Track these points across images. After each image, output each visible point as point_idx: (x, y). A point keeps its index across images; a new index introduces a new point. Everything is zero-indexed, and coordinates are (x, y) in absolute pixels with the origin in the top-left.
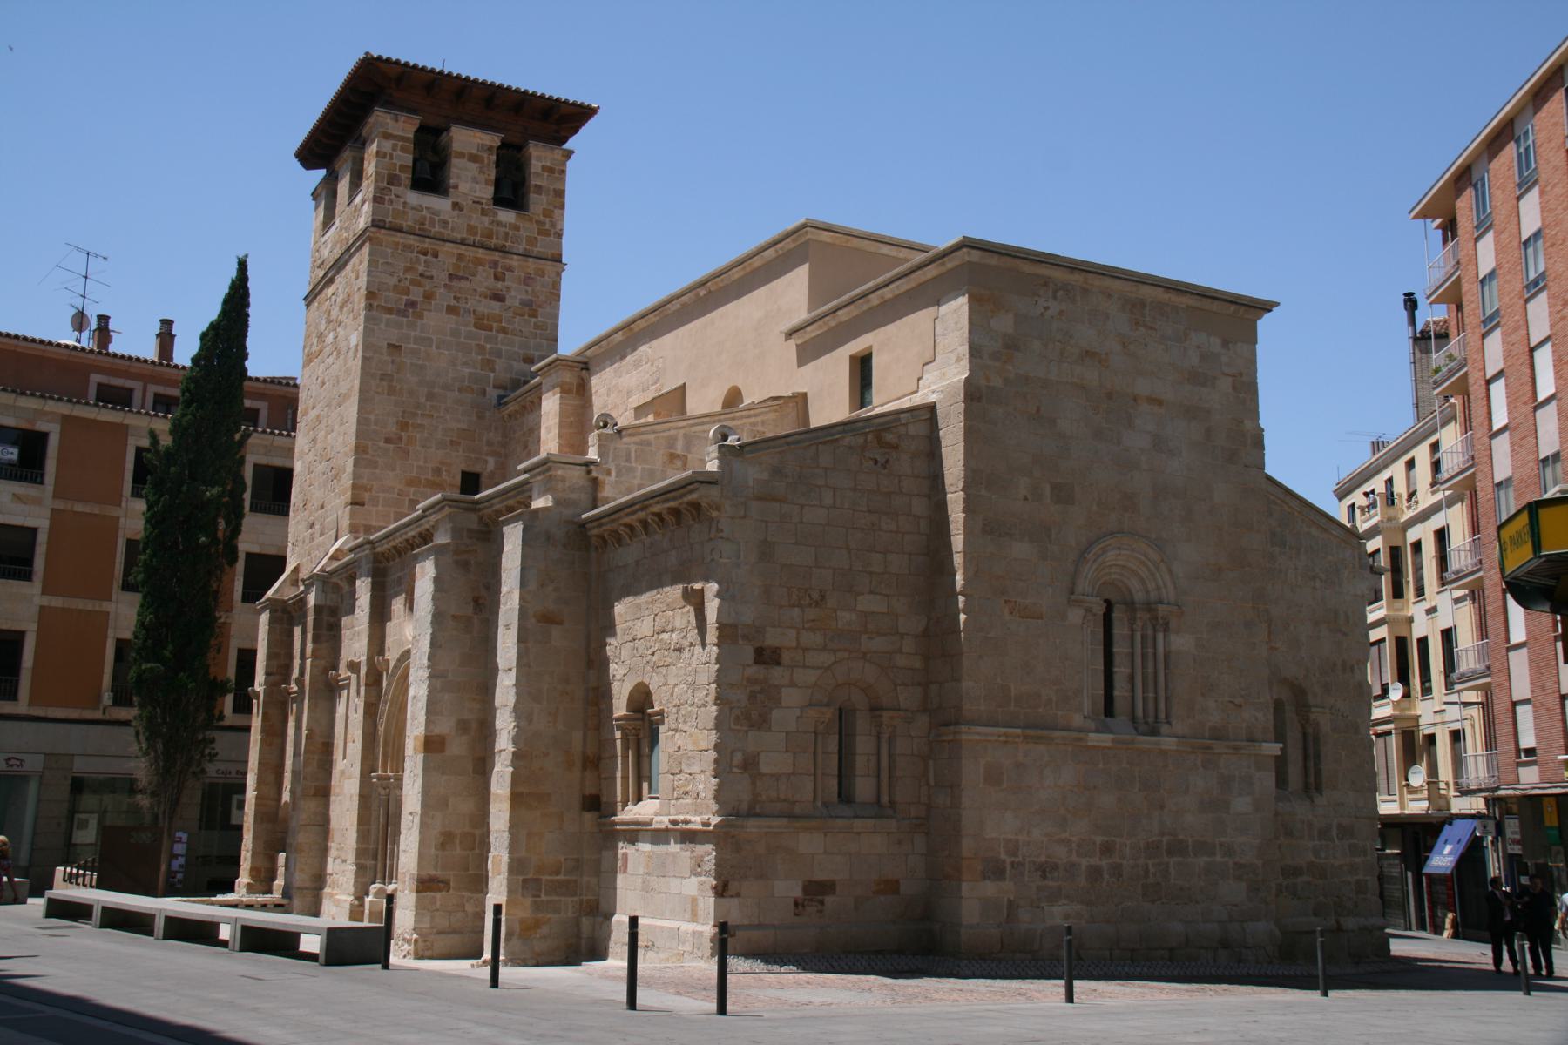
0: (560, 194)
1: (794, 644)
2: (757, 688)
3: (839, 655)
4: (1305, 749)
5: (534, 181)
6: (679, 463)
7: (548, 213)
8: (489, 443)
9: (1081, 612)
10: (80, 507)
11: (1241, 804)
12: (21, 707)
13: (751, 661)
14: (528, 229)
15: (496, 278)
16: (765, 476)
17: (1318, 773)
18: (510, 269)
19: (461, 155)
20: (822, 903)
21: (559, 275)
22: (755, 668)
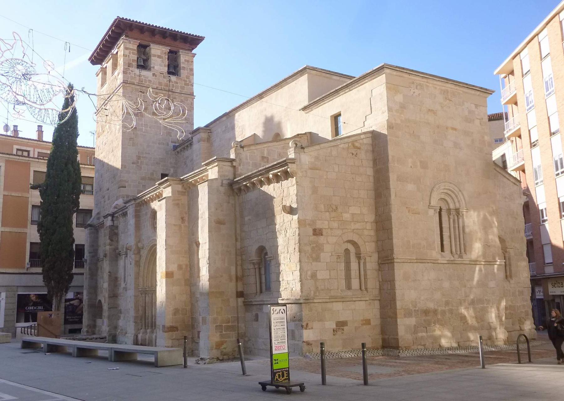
0: (192, 70)
2: (314, 245)
5: (182, 65)
6: (265, 160)
7: (188, 77)
8: (171, 163)
10: (13, 194)
14: (181, 84)
16: (313, 160)
17: (510, 271)
19: (155, 56)
20: (343, 330)
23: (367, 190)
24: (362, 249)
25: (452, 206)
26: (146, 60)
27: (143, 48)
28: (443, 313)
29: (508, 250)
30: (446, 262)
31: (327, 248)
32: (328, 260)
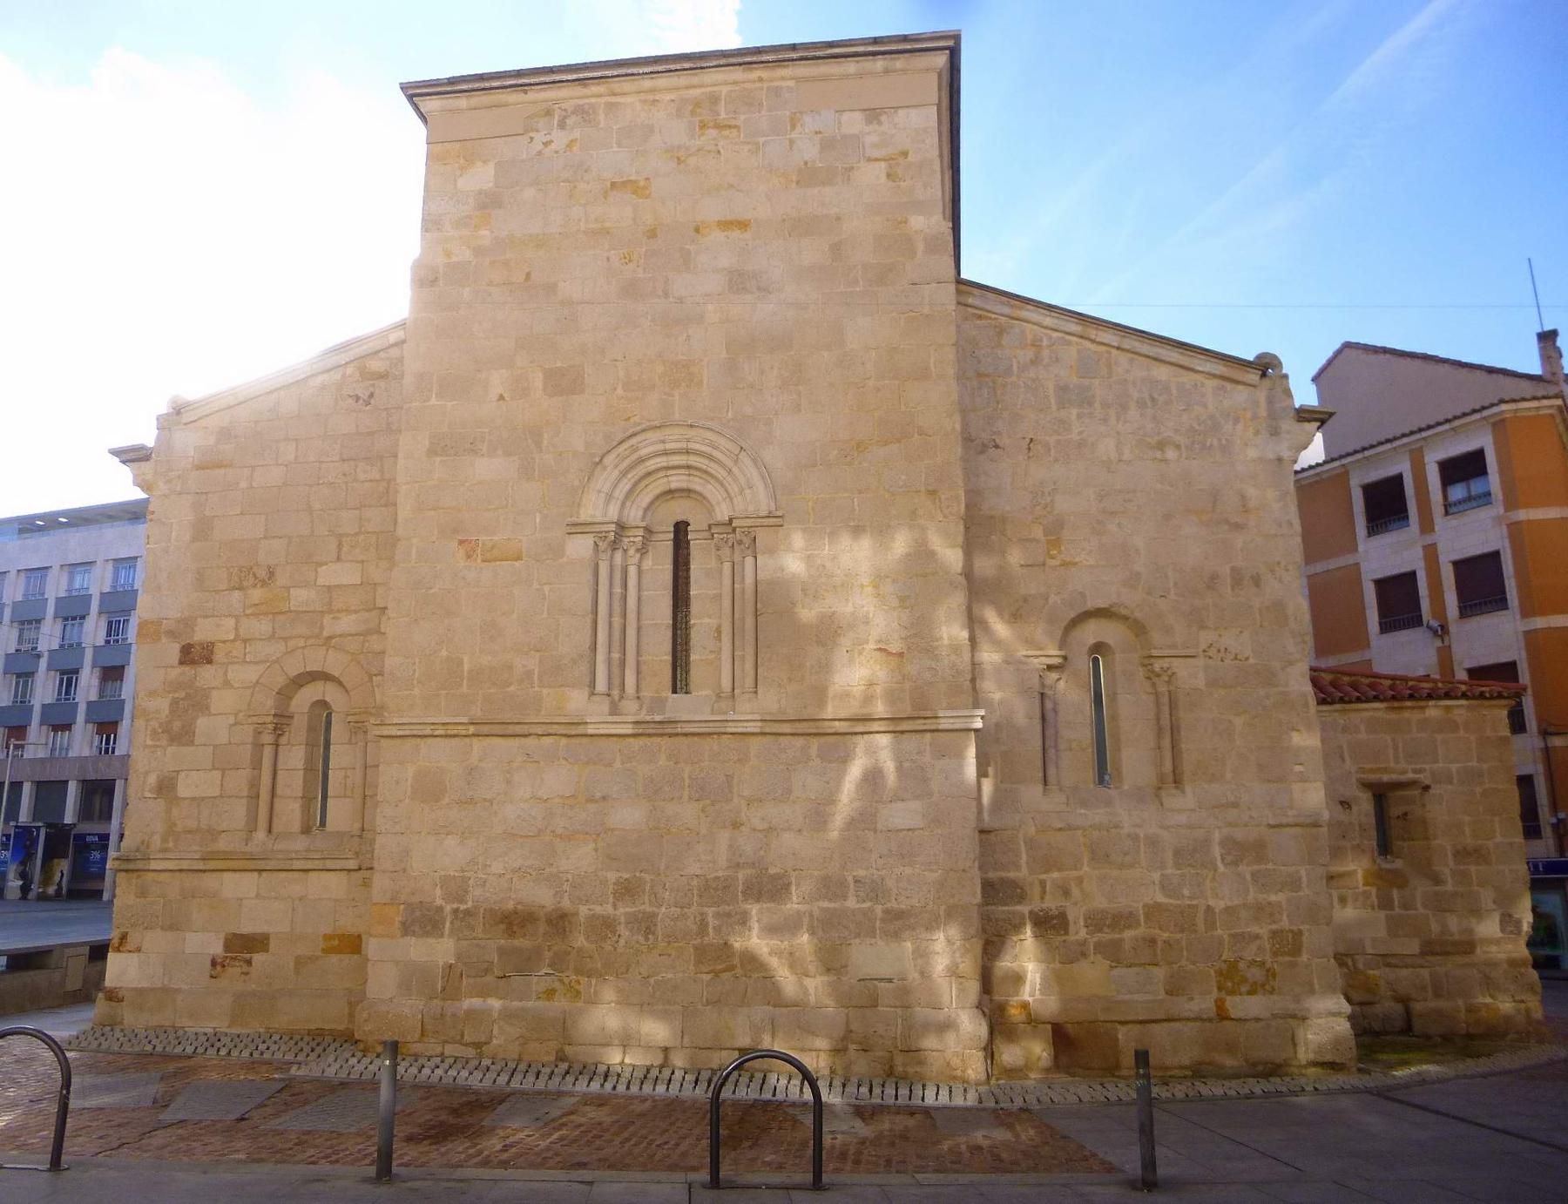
20: (249, 962)
28: (604, 927)
30: (628, 729)
31: (222, 701)
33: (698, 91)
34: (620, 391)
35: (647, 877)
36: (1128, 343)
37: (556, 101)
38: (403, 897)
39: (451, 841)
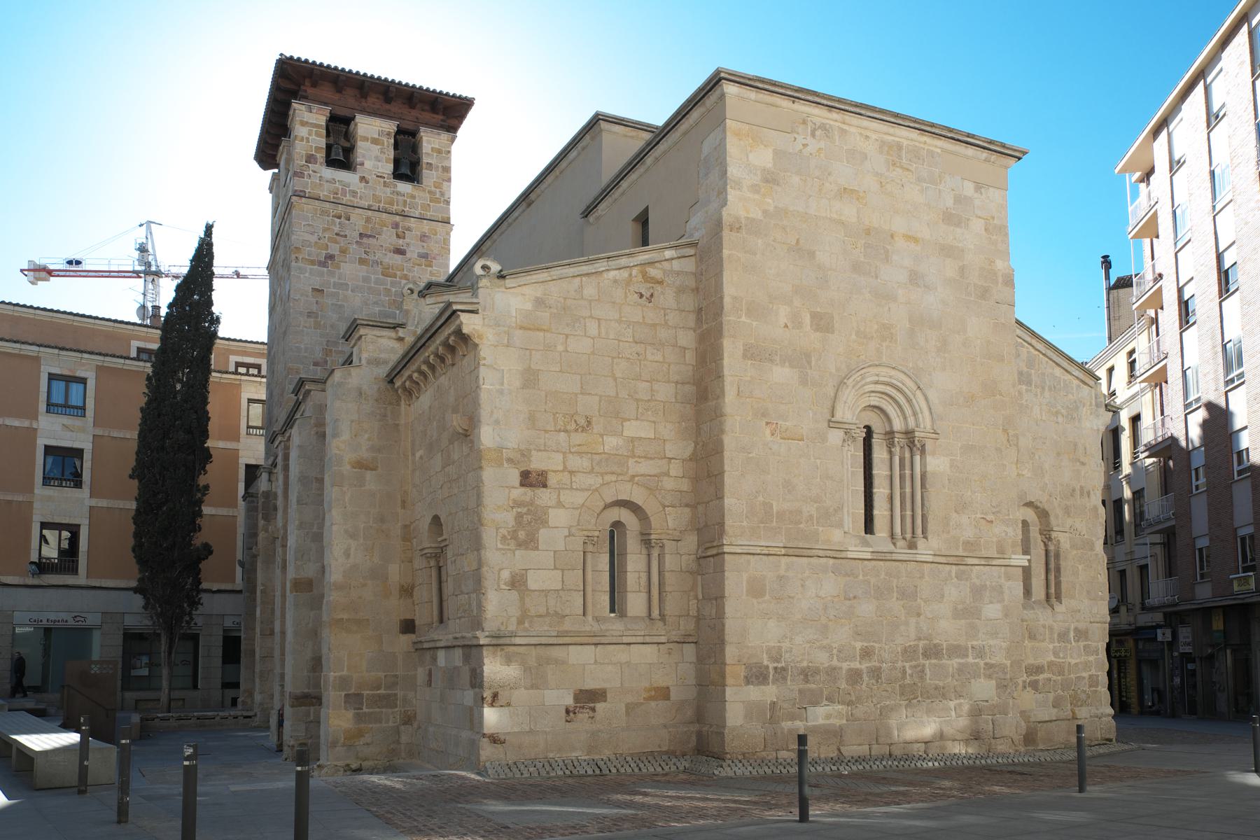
0: (447, 170)
1: (561, 468)
3: (608, 478)
4: (1047, 564)
5: (425, 160)
9: (841, 433)
10: (115, 434)
11: (992, 610)
12: (81, 579)
13: (517, 483)
15: (398, 236)
16: (529, 306)
17: (1058, 584)
18: (409, 229)
19: (366, 139)
20: (593, 710)
21: (448, 234)
22: (523, 490)
23: (677, 383)
24: (655, 522)
25: (898, 425)
26: (349, 151)
27: (339, 127)
28: (855, 676)
29: (1054, 535)
30: (869, 556)
31: (559, 518)
32: (560, 546)
33: (891, 138)
34: (854, 337)
35: (876, 645)
36: (1050, 353)
37: (809, 115)
38: (745, 660)
39: (772, 624)
